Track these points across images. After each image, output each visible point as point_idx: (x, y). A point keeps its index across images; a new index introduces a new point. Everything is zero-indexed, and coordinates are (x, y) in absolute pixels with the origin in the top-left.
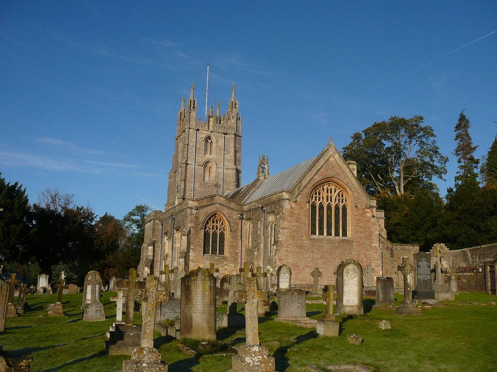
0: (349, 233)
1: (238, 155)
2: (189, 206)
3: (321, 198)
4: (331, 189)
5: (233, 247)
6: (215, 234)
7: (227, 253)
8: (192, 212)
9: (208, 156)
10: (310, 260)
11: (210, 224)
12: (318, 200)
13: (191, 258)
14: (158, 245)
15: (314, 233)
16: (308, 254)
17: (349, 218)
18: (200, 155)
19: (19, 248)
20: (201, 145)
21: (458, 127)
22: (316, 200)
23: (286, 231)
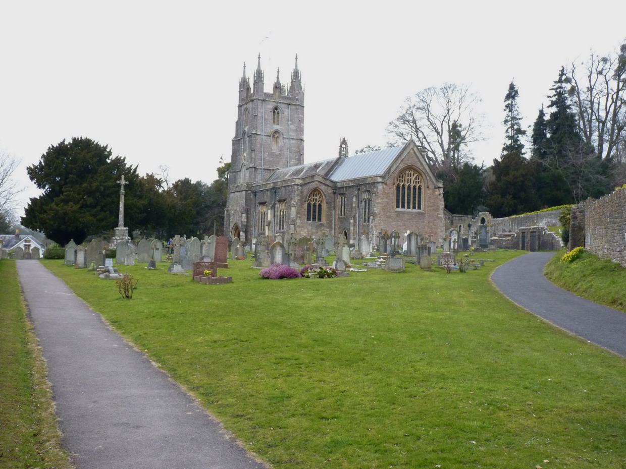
0: (422, 207)
3: (404, 181)
4: (411, 174)
5: (329, 216)
6: (315, 205)
7: (324, 220)
8: (298, 188)
9: (276, 127)
15: (398, 206)
17: (422, 196)
19: (265, 214)
23: (379, 205)
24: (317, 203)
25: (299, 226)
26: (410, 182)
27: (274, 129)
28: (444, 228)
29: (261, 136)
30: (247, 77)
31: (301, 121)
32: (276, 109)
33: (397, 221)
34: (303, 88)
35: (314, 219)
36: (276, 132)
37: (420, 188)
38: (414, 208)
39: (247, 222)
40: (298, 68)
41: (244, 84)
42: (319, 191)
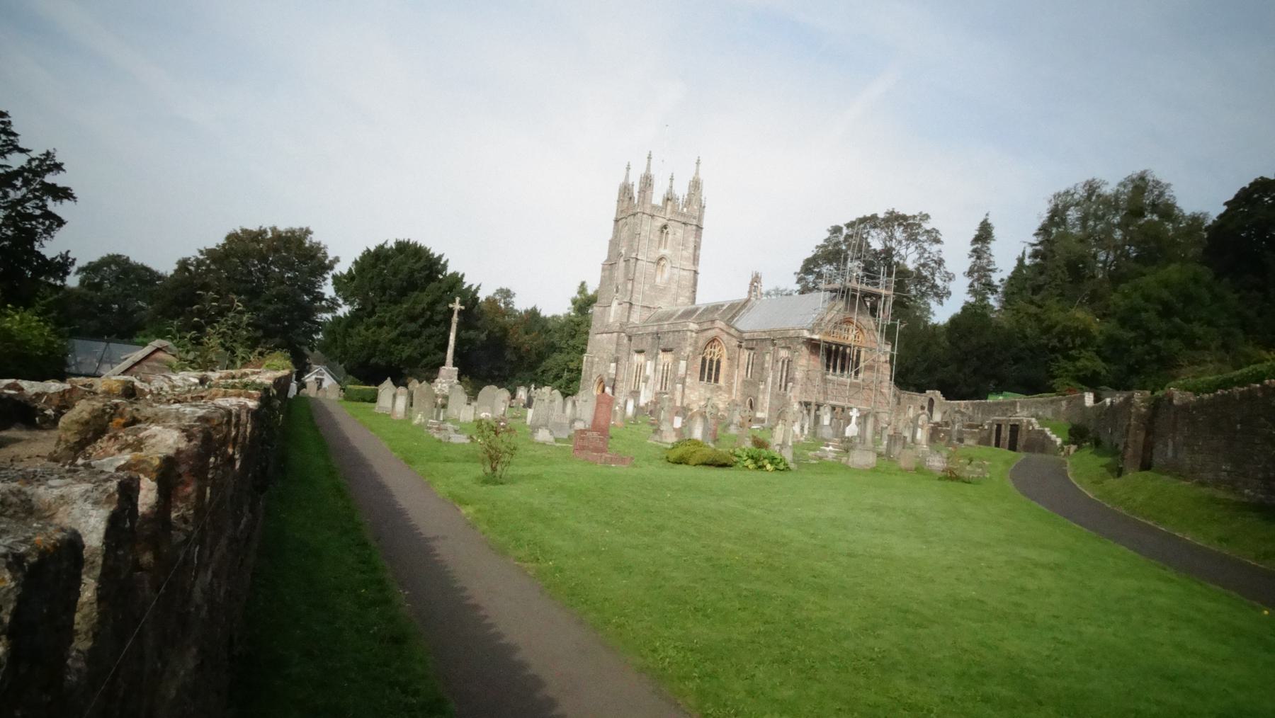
1: (698, 252)
2: (690, 328)
5: (730, 377)
6: (711, 361)
7: (722, 382)
9: (663, 252)
11: (708, 350)
13: (687, 384)
14: (623, 361)
18: (653, 248)
20: (655, 236)
21: (977, 239)
23: (802, 368)
24: (715, 359)
27: (660, 254)
32: (665, 227)
41: (625, 190)
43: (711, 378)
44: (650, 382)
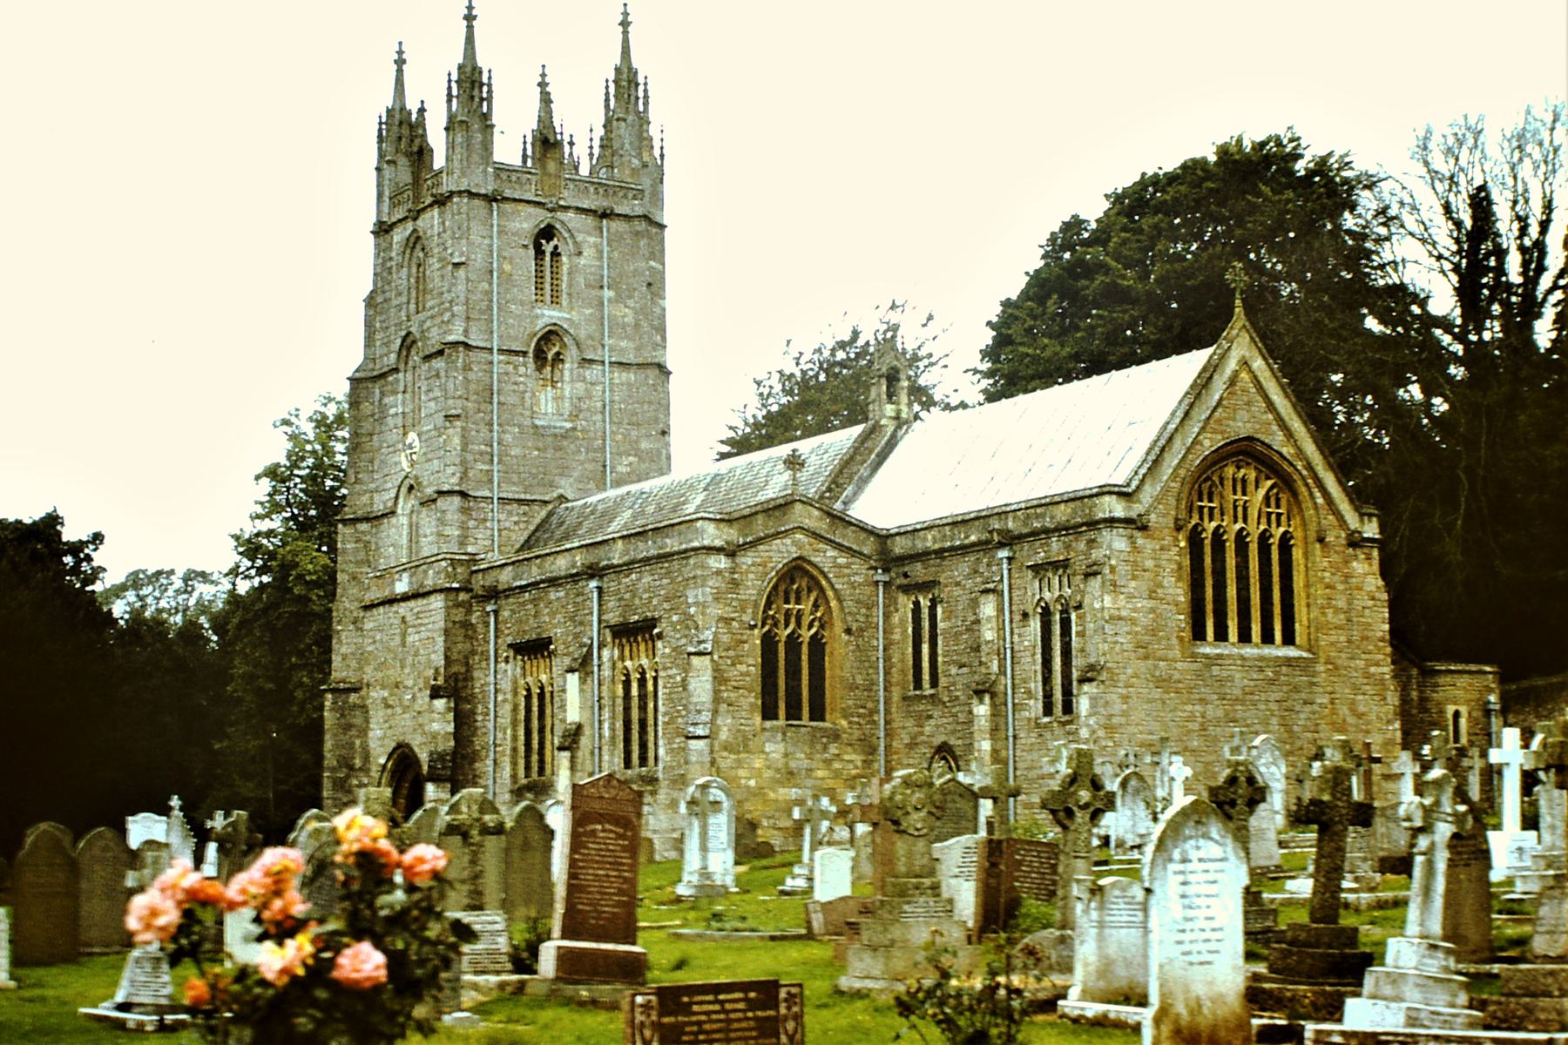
3: (1283, 518)
4: (1244, 481)
6: (1241, 538)
9: (549, 315)
10: (1196, 726)
12: (1274, 525)
16: (1189, 708)
22: (1201, 519)
24: (806, 635)
25: (726, 747)
26: (1245, 520)
27: (540, 323)
28: (1397, 725)
29: (484, 355)
30: (412, 105)
31: (655, 286)
32: (547, 233)
33: (1203, 701)
34: (657, 144)
35: (793, 713)
36: (551, 335)
37: (1285, 540)
38: (1245, 637)
39: (457, 735)
40: (636, 63)
42: (812, 577)
43: (800, 708)
44: (584, 741)
